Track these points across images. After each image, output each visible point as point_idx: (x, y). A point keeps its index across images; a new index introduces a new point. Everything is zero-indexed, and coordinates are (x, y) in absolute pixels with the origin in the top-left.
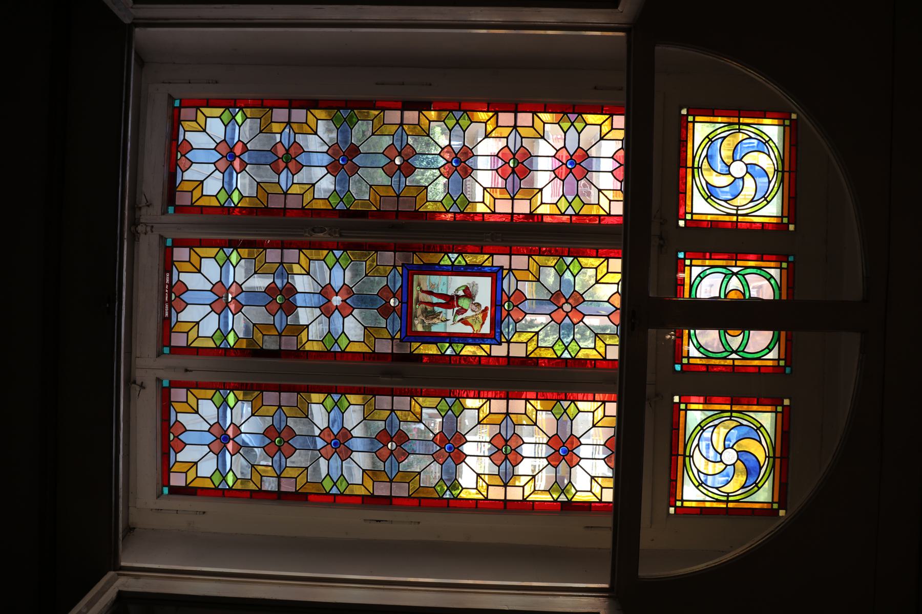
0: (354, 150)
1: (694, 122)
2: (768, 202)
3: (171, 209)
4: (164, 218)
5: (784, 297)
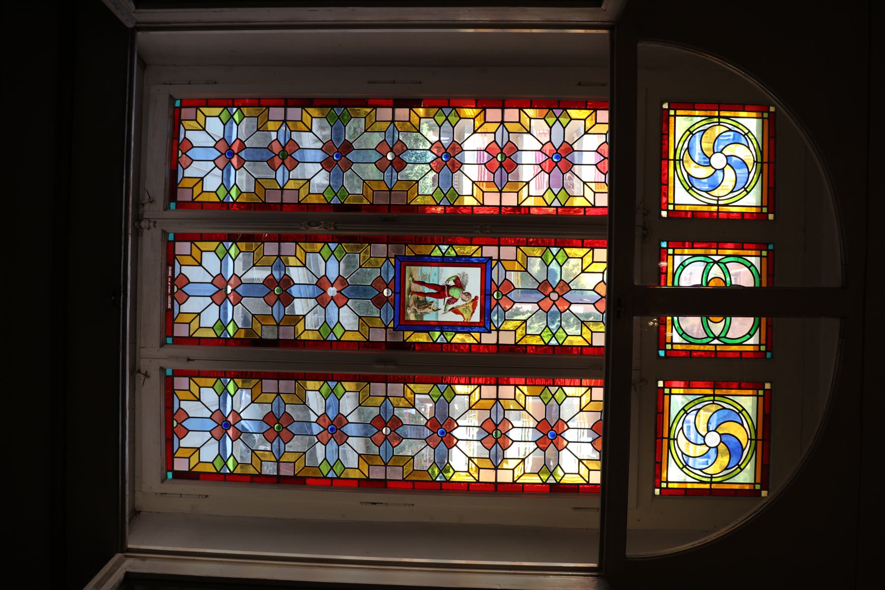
0: (348, 147)
1: (670, 394)
2: (748, 193)
3: (173, 205)
4: (167, 214)
5: (764, 285)
